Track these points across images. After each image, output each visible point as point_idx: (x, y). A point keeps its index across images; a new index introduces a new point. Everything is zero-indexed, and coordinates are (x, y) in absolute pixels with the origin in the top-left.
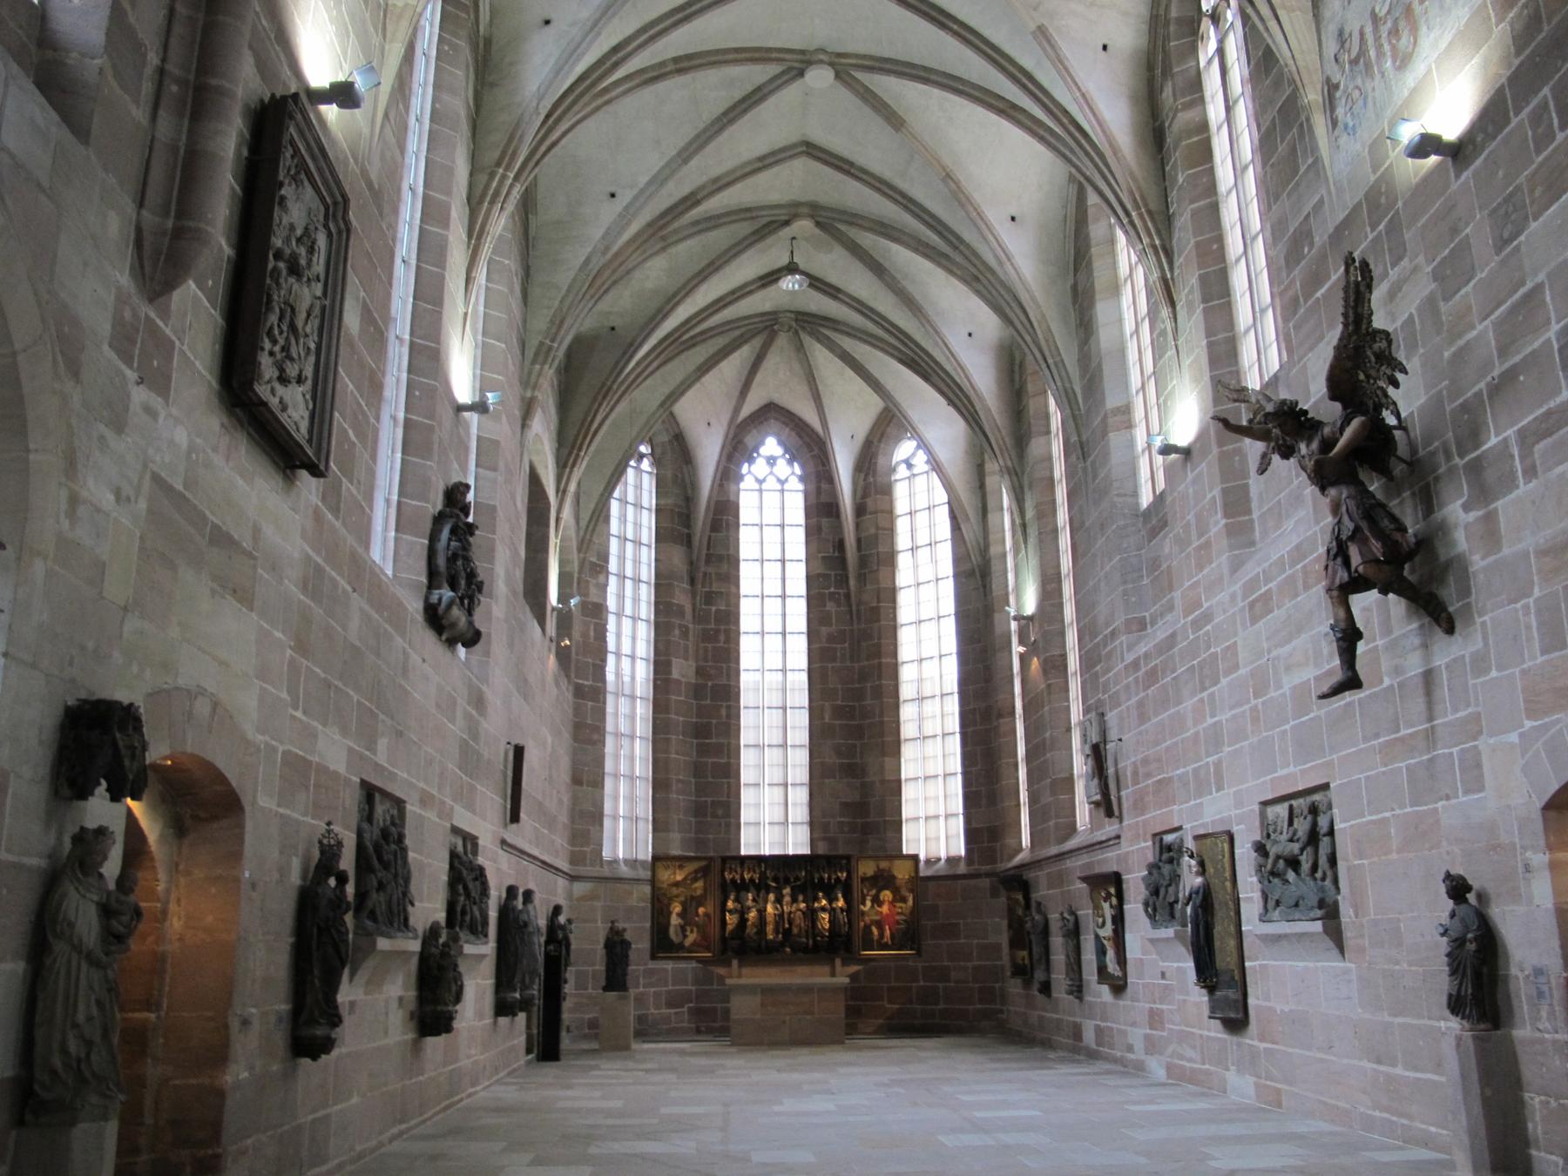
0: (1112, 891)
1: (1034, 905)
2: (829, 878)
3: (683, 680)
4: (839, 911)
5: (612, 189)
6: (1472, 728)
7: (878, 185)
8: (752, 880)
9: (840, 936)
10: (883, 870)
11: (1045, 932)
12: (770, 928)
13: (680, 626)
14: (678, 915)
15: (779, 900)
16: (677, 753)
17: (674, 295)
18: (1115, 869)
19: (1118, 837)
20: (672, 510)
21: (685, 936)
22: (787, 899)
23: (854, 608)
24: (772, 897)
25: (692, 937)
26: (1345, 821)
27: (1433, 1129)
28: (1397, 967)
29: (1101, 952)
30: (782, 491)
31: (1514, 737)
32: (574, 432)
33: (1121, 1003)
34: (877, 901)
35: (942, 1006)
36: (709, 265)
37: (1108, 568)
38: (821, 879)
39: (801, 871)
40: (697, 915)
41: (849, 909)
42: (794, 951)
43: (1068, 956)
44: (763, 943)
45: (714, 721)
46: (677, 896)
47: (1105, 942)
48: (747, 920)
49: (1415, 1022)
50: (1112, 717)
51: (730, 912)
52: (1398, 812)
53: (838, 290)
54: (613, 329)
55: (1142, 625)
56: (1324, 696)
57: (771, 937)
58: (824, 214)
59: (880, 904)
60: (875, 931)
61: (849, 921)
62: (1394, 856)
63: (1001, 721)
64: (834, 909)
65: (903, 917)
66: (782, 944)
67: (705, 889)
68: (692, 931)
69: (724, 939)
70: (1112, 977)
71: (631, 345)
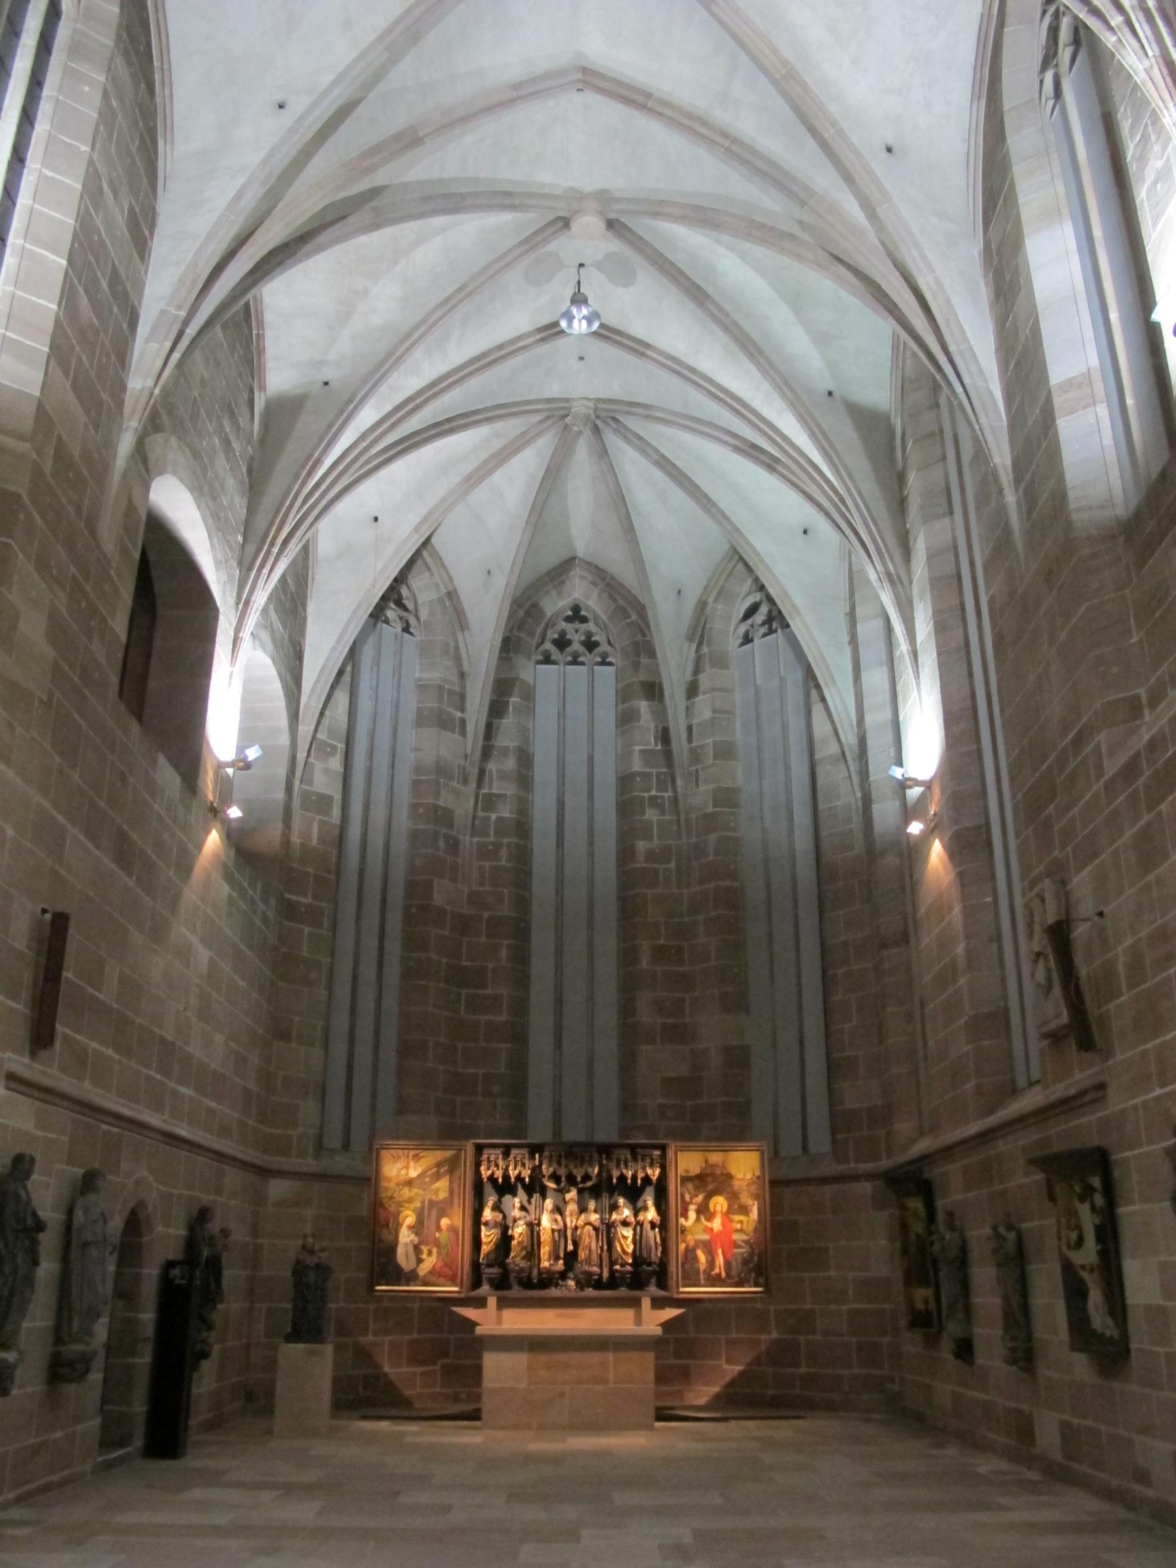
0: (1096, 1182)
1: (941, 1217)
2: (634, 1177)
3: (448, 908)
4: (647, 1226)
5: (279, 97)
7: (688, 122)
8: (519, 1178)
9: (650, 1264)
10: (714, 1166)
11: (962, 1260)
12: (545, 1250)
13: (446, 837)
14: (410, 1228)
15: (559, 1210)
16: (434, 1006)
17: (410, 333)
18: (1095, 1141)
19: (1101, 1086)
20: (440, 688)
21: (420, 1261)
22: (572, 1207)
23: (682, 816)
24: (549, 1203)
25: (429, 1262)
29: (1075, 1293)
32: (264, 525)
33: (1116, 1385)
34: (704, 1211)
35: (803, 1370)
36: (459, 290)
37: (1063, 636)
38: (622, 1178)
39: (591, 1165)
40: (439, 1229)
41: (663, 1226)
42: (580, 1285)
43: (1006, 1298)
44: (535, 1273)
45: (491, 966)
46: (410, 1200)
47: (1085, 1275)
48: (512, 1238)
50: (1081, 882)
51: (486, 1224)
53: (647, 345)
54: (326, 384)
55: (1134, 709)
57: (545, 1264)
58: (617, 207)
59: (710, 1217)
60: (702, 1256)
61: (664, 1241)
63: (885, 953)
64: (640, 1224)
65: (745, 1237)
66: (563, 1275)
67: (451, 1192)
68: (430, 1253)
69: (476, 1266)
70: (1100, 1337)
71: (350, 401)
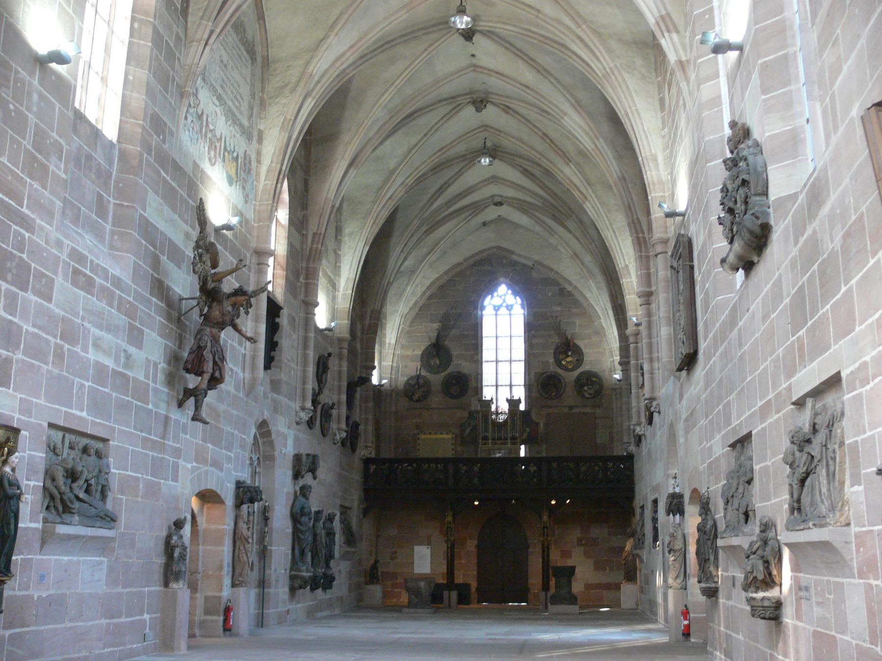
31: (189, 466)
52: (145, 476)
56: (246, 151)
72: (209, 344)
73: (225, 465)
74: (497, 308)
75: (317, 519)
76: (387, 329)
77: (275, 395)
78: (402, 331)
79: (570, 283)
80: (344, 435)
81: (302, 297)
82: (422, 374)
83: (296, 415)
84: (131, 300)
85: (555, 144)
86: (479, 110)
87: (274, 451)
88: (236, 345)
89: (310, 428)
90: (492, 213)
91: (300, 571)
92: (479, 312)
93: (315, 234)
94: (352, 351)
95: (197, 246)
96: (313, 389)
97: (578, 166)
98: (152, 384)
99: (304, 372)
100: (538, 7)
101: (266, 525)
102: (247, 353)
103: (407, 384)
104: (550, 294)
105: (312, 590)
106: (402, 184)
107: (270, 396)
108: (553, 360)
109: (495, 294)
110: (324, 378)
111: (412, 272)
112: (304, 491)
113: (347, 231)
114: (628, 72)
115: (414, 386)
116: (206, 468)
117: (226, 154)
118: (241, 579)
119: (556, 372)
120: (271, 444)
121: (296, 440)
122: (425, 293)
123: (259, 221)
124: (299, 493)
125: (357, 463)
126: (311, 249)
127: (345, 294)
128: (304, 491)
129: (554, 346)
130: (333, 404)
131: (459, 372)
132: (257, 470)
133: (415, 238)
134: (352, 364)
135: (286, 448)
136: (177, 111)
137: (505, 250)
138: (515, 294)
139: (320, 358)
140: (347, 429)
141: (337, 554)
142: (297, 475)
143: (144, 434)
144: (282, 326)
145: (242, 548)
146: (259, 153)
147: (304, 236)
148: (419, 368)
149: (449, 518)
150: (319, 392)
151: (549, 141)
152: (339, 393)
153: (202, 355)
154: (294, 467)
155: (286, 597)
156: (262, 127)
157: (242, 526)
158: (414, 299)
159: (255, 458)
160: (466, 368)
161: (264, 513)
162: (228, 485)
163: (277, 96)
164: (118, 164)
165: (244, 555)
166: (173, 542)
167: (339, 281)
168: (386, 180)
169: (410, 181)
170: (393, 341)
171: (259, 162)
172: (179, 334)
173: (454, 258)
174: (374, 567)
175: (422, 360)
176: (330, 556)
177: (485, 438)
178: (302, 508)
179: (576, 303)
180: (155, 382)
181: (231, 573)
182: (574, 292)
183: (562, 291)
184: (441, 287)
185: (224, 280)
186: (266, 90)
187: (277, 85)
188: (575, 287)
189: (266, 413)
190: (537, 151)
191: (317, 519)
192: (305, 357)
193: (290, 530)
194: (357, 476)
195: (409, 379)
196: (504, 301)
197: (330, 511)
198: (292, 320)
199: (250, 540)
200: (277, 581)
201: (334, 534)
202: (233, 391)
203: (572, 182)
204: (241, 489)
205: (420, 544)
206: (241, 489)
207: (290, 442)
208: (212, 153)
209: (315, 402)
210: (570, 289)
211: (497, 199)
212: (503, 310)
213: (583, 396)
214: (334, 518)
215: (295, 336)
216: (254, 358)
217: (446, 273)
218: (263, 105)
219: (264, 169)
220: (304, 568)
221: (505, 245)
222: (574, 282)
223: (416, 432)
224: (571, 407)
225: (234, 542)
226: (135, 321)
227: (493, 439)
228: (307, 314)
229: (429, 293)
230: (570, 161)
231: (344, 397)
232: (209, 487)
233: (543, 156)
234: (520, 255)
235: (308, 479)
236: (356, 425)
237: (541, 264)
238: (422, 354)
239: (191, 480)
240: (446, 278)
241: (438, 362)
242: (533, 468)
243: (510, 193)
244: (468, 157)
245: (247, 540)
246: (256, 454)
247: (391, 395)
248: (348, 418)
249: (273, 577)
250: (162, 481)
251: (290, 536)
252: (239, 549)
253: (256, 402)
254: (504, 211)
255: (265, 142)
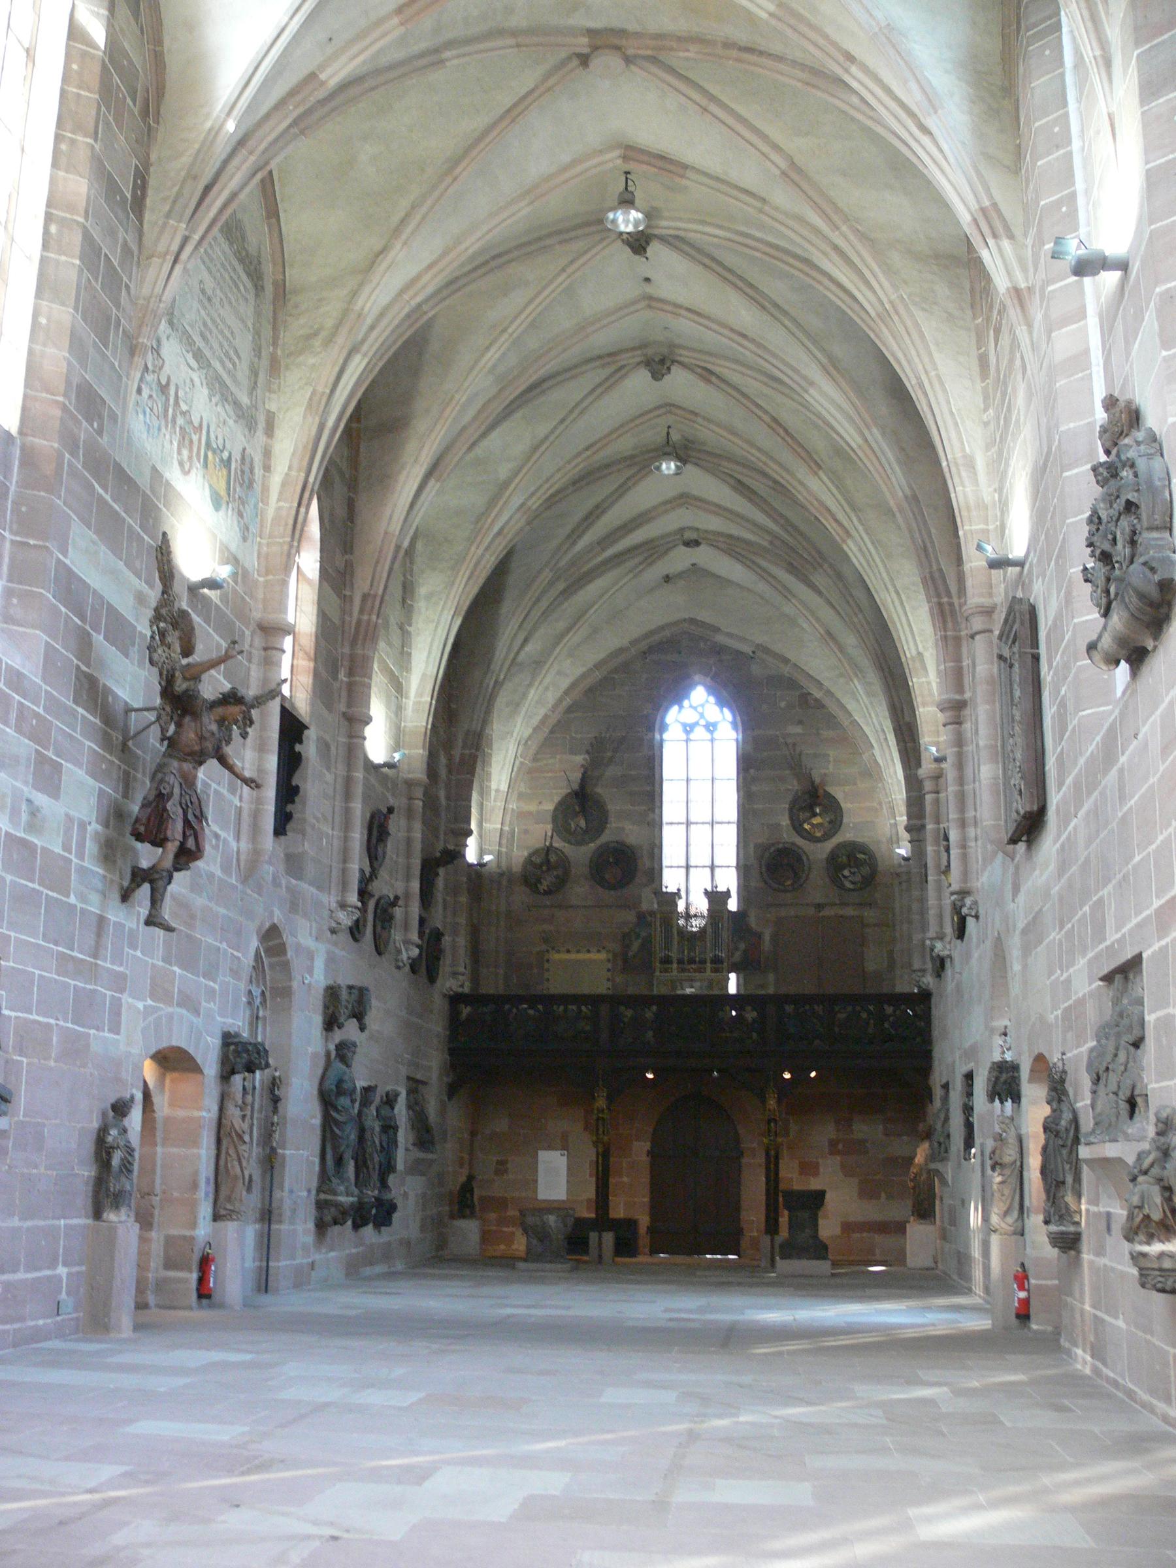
6: (119, 983)
26: (11, 1010)
27: (41, 1322)
28: (35, 1171)
30: (712, 740)
31: (140, 1005)
49: (42, 1223)
52: (61, 1023)
56: (244, 449)
62: (52, 1063)
72: (177, 791)
73: (204, 1003)
74: (688, 729)
75: (365, 1103)
76: (494, 765)
77: (293, 881)
78: (519, 769)
79: (819, 684)
80: (416, 952)
81: (342, 707)
82: (555, 845)
83: (331, 917)
84: (41, 711)
85: (792, 437)
86: (657, 376)
87: (290, 979)
88: (225, 792)
89: (355, 939)
90: (680, 559)
91: (335, 1194)
92: (657, 736)
93: (365, 597)
94: (431, 803)
95: (158, 617)
96: (362, 871)
97: (837, 479)
98: (75, 860)
99: (346, 839)
100: (764, 195)
101: (275, 1110)
102: (245, 806)
103: (529, 861)
104: (783, 704)
105: (356, 1227)
106: (518, 509)
107: (284, 882)
108: (788, 822)
109: (686, 703)
110: (380, 850)
111: (538, 664)
112: (344, 1052)
113: (422, 591)
114: (924, 310)
115: (541, 866)
116: (170, 1010)
117: (210, 454)
118: (229, 1206)
119: (793, 844)
120: (286, 966)
121: (331, 960)
122: (560, 700)
123: (267, 573)
124: (333, 1054)
125: (439, 1004)
126: (359, 622)
127: (419, 703)
128: (344, 1052)
129: (790, 798)
130: (397, 898)
131: (623, 844)
132: (261, 1014)
133: (544, 604)
134: (430, 826)
135: (311, 975)
136: (124, 379)
137: (703, 624)
138: (721, 703)
139: (373, 817)
140: (419, 942)
141: (400, 1166)
142: (331, 1023)
143: (60, 949)
144: (307, 759)
145: (231, 1151)
146: (267, 453)
147: (346, 600)
148: (549, 834)
149: (601, 1103)
150: (371, 877)
151: (781, 432)
152: (408, 878)
153: (165, 809)
154: (326, 1007)
155: (310, 1239)
156: (273, 407)
157: (233, 1113)
158: (542, 711)
159: (257, 992)
160: (632, 834)
161: (272, 1091)
162: (209, 1039)
163: (301, 352)
164: (19, 473)
165: (236, 1163)
166: (110, 1139)
167: (408, 680)
168: (492, 502)
169: (535, 503)
170: (504, 787)
171: (267, 468)
172: (125, 771)
173: (613, 640)
174: (467, 1189)
175: (554, 820)
176: (388, 1168)
177: (667, 961)
178: (340, 1083)
179: (831, 721)
180: (81, 856)
181: (211, 1196)
182: (827, 701)
183: (805, 699)
184: (590, 690)
185: (205, 677)
186: (280, 342)
187: (301, 332)
188: (829, 693)
189: (277, 912)
190: (759, 449)
191: (365, 1103)
192: (347, 812)
193: (317, 1121)
194: (437, 1026)
195: (530, 855)
196: (702, 715)
197: (389, 1088)
198: (324, 747)
199: (247, 1138)
200: (294, 1211)
201: (396, 1128)
202: (218, 873)
203: (821, 503)
204: (232, 1047)
205: (550, 1148)
206: (232, 1047)
207: (319, 964)
208: (185, 452)
209: (363, 894)
210: (818, 694)
211: (688, 535)
212: (700, 733)
213: (841, 887)
214: (396, 1100)
215: (329, 777)
216: (256, 815)
217: (597, 666)
218: (275, 367)
219: (276, 480)
220: (342, 1188)
221: (704, 616)
222: (826, 683)
223: (544, 947)
224: (820, 907)
225: (219, 1142)
226: (47, 749)
227: (680, 962)
228: (351, 736)
229: (568, 701)
230: (820, 467)
231: (415, 885)
232: (174, 1043)
233: (771, 458)
234: (730, 635)
235: (350, 1030)
236: (437, 935)
237: (766, 650)
238: (556, 809)
239: (144, 1030)
240: (598, 675)
241: (583, 823)
242: (751, 1015)
243: (713, 523)
244: (636, 460)
245: (240, 1137)
246: (258, 986)
247: (499, 883)
248: (422, 921)
249: (287, 1205)
250: (92, 1031)
251: (318, 1132)
252: (227, 1153)
253: (260, 894)
254: (704, 556)
255: (279, 433)
